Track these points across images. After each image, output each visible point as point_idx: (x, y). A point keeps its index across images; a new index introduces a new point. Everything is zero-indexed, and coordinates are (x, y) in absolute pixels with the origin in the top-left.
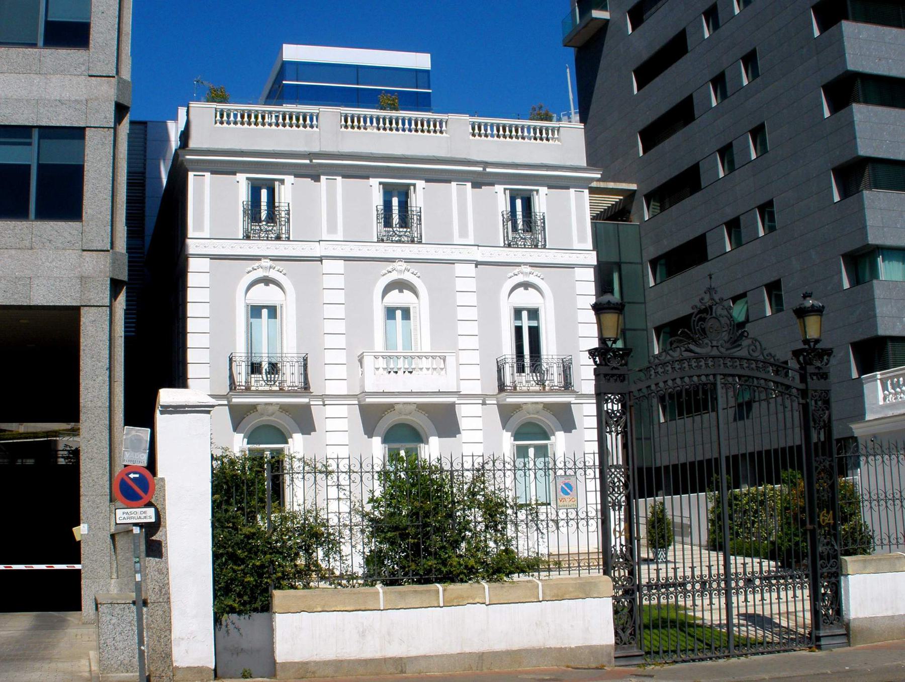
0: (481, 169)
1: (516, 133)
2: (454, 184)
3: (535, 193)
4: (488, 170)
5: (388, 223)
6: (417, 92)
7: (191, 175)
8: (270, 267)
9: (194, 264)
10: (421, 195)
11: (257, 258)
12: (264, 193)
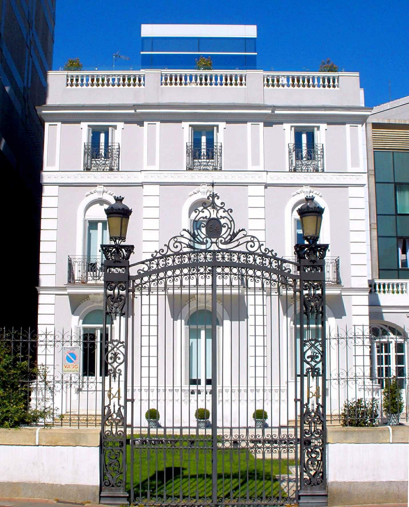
0: (270, 112)
1: (308, 83)
2: (348, 126)
3: (316, 129)
4: (276, 112)
5: (299, 157)
6: (245, 55)
7: (47, 125)
8: (104, 192)
9: (47, 191)
10: (323, 135)
11: (94, 185)
12: (304, 137)
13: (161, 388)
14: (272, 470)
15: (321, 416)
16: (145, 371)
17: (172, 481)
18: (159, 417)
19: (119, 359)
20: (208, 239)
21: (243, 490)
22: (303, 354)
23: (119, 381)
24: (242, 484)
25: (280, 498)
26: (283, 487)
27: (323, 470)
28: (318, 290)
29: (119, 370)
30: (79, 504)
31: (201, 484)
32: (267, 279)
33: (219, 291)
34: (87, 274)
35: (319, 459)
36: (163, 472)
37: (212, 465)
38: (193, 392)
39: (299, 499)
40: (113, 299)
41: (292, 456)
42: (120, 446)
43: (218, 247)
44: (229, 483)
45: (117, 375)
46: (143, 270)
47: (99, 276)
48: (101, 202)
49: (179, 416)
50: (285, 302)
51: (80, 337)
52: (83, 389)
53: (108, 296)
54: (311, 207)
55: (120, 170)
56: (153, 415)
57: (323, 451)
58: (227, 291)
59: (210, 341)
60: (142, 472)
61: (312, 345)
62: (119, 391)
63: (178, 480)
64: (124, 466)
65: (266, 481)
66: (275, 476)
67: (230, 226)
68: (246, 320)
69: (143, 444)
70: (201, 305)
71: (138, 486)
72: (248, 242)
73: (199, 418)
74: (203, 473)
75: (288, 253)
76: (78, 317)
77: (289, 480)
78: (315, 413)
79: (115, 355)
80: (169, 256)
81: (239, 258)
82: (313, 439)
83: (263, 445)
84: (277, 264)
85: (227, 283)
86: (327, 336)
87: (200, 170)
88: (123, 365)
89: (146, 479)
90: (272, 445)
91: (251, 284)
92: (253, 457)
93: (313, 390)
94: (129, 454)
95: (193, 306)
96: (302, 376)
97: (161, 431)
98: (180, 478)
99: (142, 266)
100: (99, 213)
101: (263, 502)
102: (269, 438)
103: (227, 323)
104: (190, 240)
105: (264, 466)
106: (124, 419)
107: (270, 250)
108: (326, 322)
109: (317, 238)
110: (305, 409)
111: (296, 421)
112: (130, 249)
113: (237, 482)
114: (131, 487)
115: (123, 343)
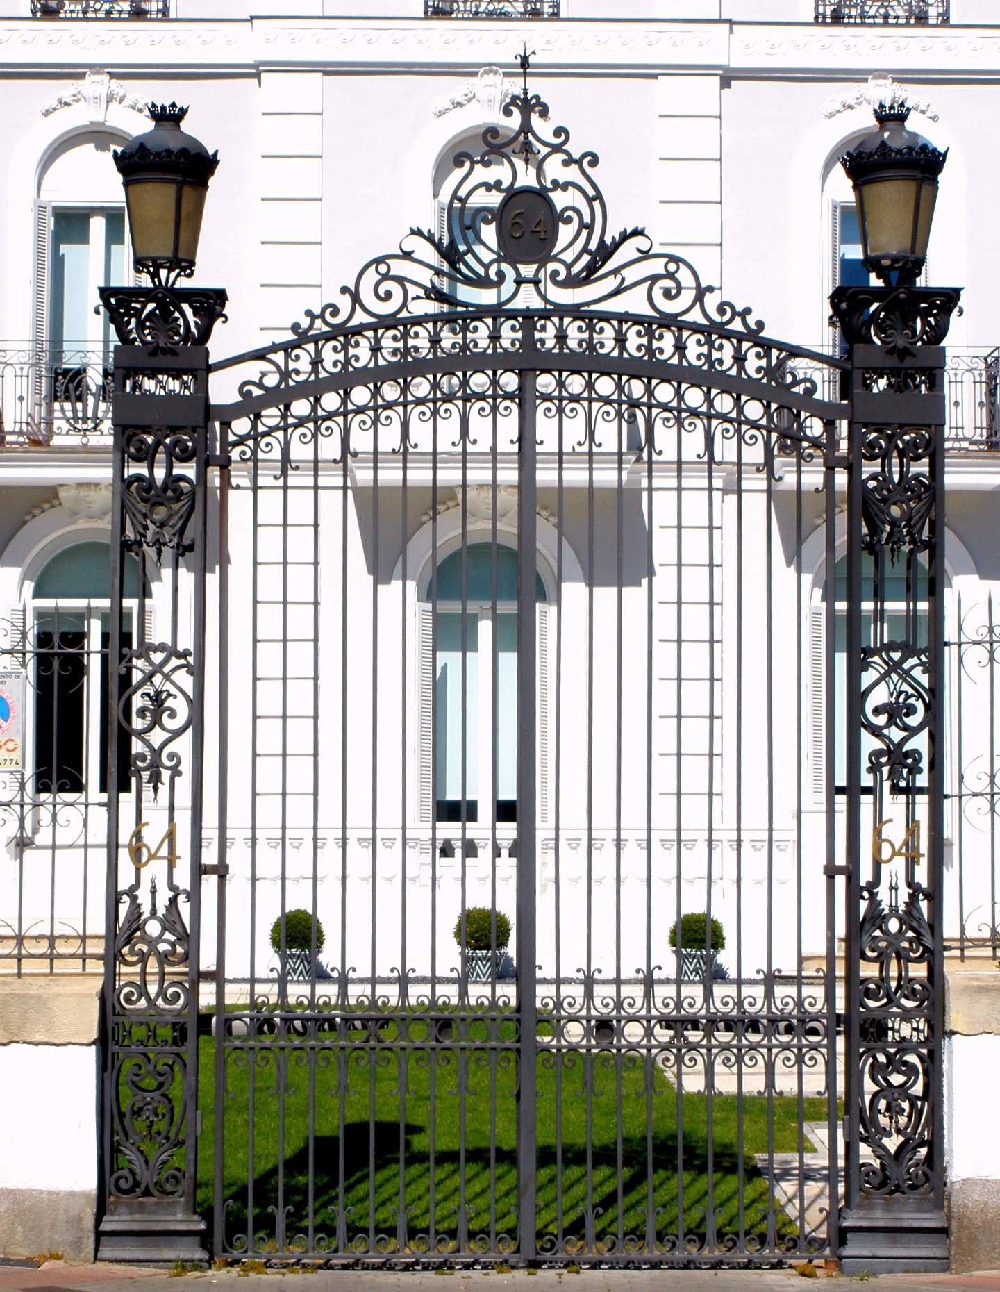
8: (110, 99)
13: (330, 833)
14: (740, 1134)
15: (926, 932)
16: (269, 771)
17: (367, 1176)
18: (320, 941)
19: (173, 715)
20: (505, 267)
21: (633, 1206)
22: (857, 697)
23: (172, 808)
24: (629, 1186)
25: (771, 1237)
26: (783, 1200)
27: (932, 1135)
28: (917, 458)
29: (172, 756)
30: (19, 1263)
31: (477, 1187)
32: (725, 418)
33: (545, 476)
34: (50, 411)
35: (918, 1089)
36: (334, 1140)
37: (518, 1108)
38: (447, 851)
39: (843, 1242)
40: (148, 490)
41: (815, 1083)
42: (175, 1042)
43: (543, 297)
44: (578, 1181)
45: (166, 775)
46: (260, 385)
47: (95, 417)
48: (98, 135)
49: (396, 935)
50: (794, 517)
51: (24, 635)
52: (38, 840)
53: (126, 483)
54: (895, 144)
55: (172, 15)
56: (298, 934)
57: (933, 1063)
58: (576, 476)
59: (509, 660)
60: (256, 1144)
61: (894, 667)
62: (171, 836)
63: (394, 1168)
64: (189, 1115)
65: (719, 1175)
66: (751, 1158)
67: (587, 219)
68: (645, 581)
69: (260, 1031)
70: (479, 528)
71: (240, 1195)
72: (654, 278)
73: (468, 944)
74: (483, 1144)
75: (807, 323)
76: (16, 572)
77: (806, 1175)
78: (901, 920)
79: (158, 700)
80: (359, 330)
81: (621, 340)
82: (896, 1015)
83: (709, 1035)
84: (763, 363)
85: (577, 438)
86: (950, 633)
87: (476, 16)
88: (186, 740)
89: (270, 1166)
90: (739, 1036)
91: (665, 437)
92: (666, 1083)
93: (895, 832)
94: (207, 1081)
95: (449, 530)
96: (853, 791)
97: (327, 991)
98: (397, 1161)
99: (252, 370)
100: (96, 180)
101: (706, 1252)
102: (730, 1010)
103: (574, 592)
104: (438, 272)
105: (710, 1122)
106: (190, 939)
107: (739, 309)
108: (947, 591)
109: (916, 264)
110: (864, 905)
111: (831, 957)
112: (211, 304)
113: (610, 1177)
114: (214, 1196)
115: (185, 655)
